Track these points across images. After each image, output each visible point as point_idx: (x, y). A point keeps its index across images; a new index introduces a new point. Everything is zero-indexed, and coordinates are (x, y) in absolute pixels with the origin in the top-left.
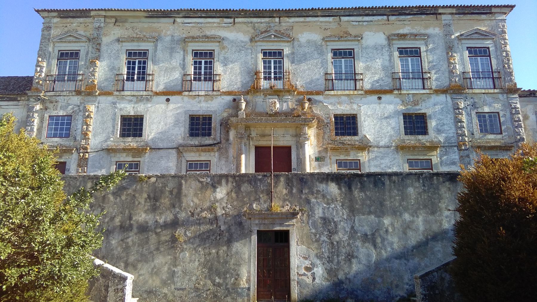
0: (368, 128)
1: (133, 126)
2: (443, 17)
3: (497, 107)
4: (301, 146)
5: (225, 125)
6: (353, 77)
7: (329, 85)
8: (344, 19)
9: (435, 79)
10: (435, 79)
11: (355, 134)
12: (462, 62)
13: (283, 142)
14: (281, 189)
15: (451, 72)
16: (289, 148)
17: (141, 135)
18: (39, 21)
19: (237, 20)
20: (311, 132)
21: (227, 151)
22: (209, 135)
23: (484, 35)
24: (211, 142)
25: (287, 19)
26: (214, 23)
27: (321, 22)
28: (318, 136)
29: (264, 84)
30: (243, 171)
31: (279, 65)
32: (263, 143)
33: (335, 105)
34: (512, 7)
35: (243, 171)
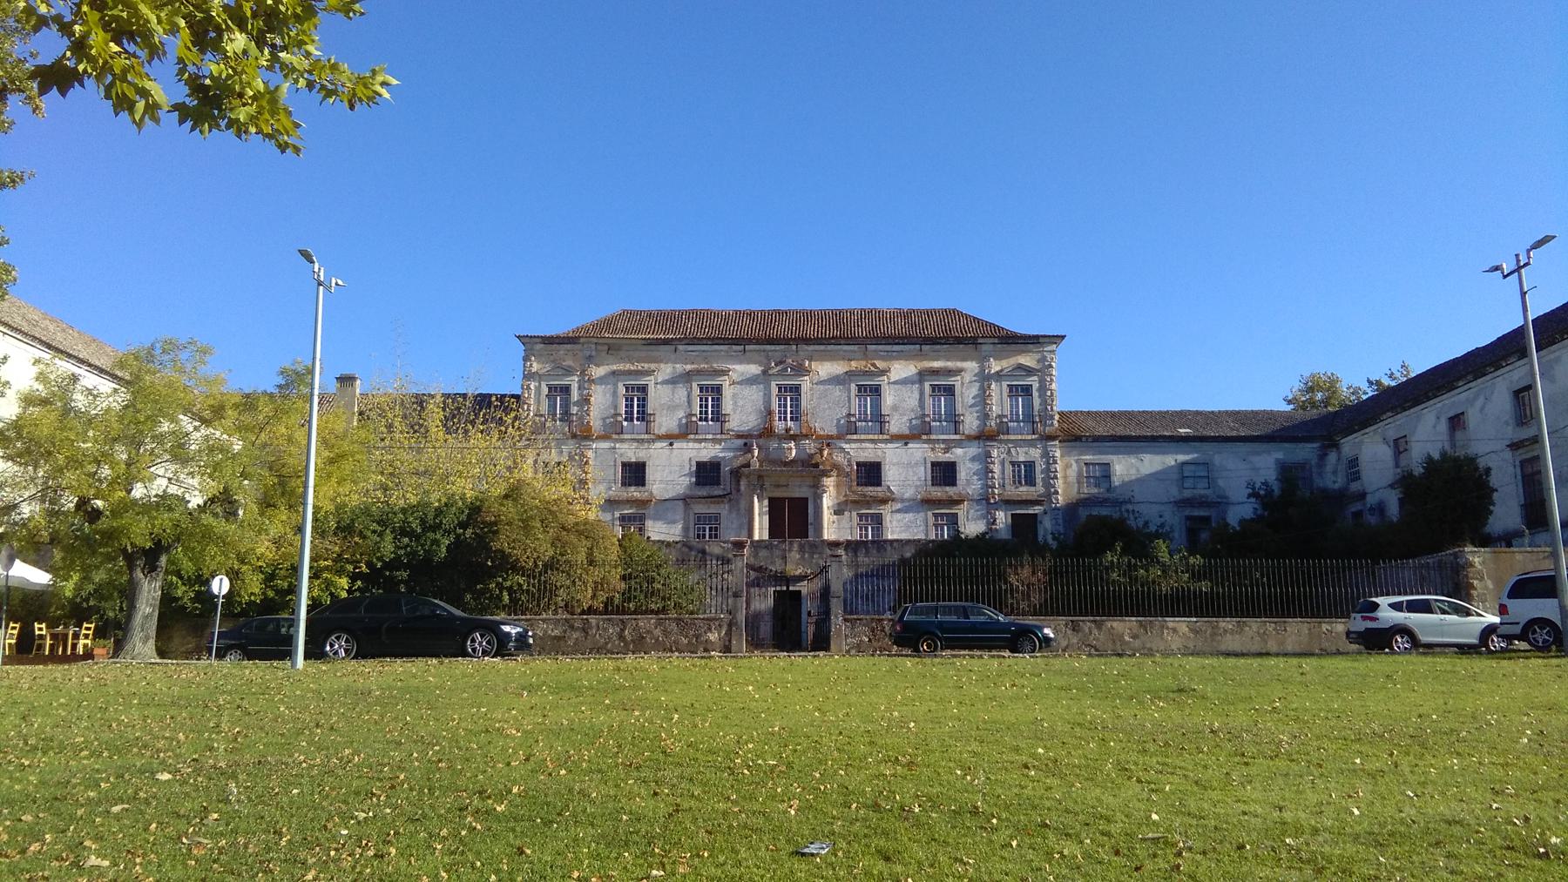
0: (893, 477)
1: (635, 473)
2: (984, 347)
3: (1035, 453)
4: (818, 498)
5: (736, 474)
6: (879, 419)
7: (849, 429)
9: (971, 423)
10: (971, 423)
11: (879, 484)
12: (999, 401)
13: (797, 493)
14: (795, 555)
15: (986, 416)
16: (806, 499)
17: (643, 485)
18: (520, 349)
20: (829, 482)
21: (738, 502)
22: (718, 484)
23: (1029, 371)
28: (838, 486)
29: (779, 426)
30: (756, 537)
31: (796, 402)
32: (778, 494)
33: (858, 451)
34: (1063, 337)
35: (756, 537)
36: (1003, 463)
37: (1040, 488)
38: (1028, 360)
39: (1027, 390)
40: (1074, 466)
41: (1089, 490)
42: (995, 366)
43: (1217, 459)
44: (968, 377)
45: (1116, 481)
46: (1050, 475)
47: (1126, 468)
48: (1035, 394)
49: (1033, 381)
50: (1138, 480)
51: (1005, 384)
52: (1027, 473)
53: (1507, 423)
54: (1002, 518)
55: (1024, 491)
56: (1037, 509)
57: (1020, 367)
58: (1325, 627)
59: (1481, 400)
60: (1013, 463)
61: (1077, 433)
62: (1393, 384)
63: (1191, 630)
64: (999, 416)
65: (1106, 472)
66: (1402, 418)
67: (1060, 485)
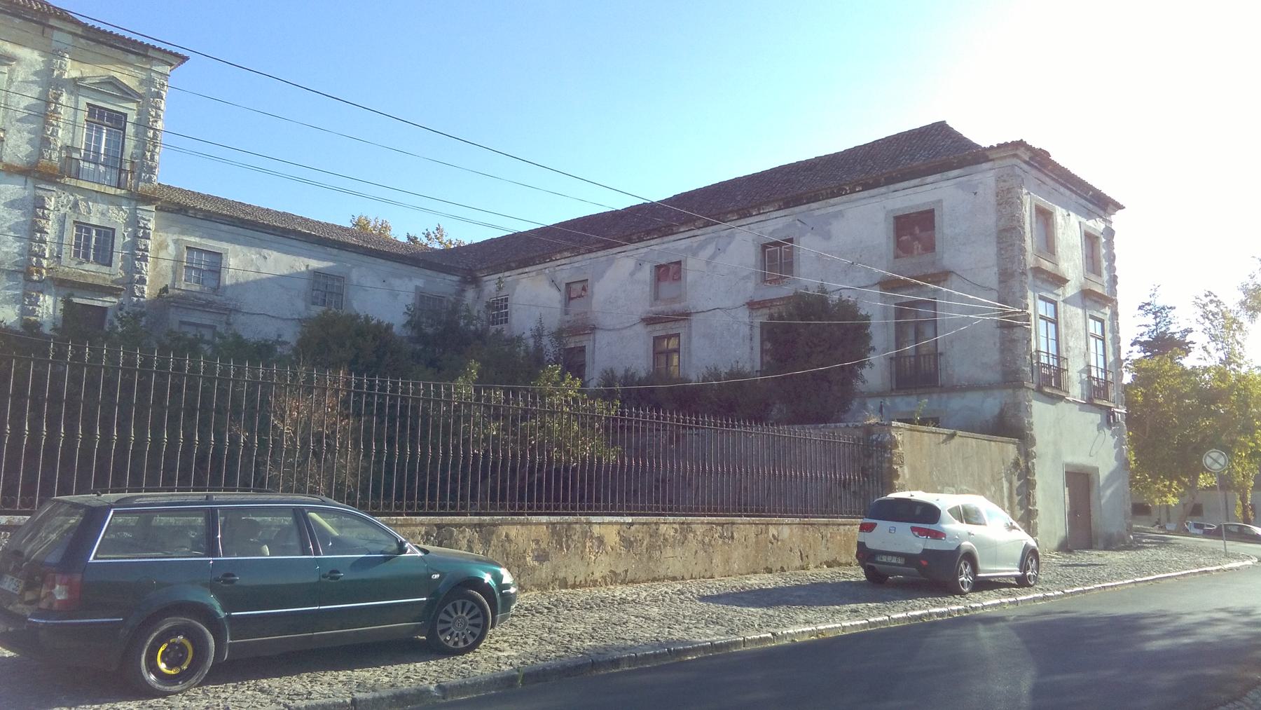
2: (57, 35)
3: (117, 217)
15: (45, 142)
23: (126, 93)
34: (184, 59)
36: (62, 222)
37: (117, 269)
38: (128, 77)
39: (118, 121)
40: (172, 249)
41: (186, 285)
42: (72, 70)
43: (355, 275)
44: (21, 73)
45: (228, 279)
46: (136, 253)
47: (243, 263)
48: (130, 129)
49: (131, 110)
50: (255, 282)
51: (83, 102)
52: (99, 244)
53: (746, 278)
54: (47, 306)
55: (91, 270)
56: (109, 301)
57: (113, 82)
58: (772, 530)
59: (710, 250)
60: (79, 225)
61: (183, 209)
62: (437, 246)
63: (623, 539)
64: (69, 148)
65: (216, 262)
66: (583, 261)
67: (148, 269)
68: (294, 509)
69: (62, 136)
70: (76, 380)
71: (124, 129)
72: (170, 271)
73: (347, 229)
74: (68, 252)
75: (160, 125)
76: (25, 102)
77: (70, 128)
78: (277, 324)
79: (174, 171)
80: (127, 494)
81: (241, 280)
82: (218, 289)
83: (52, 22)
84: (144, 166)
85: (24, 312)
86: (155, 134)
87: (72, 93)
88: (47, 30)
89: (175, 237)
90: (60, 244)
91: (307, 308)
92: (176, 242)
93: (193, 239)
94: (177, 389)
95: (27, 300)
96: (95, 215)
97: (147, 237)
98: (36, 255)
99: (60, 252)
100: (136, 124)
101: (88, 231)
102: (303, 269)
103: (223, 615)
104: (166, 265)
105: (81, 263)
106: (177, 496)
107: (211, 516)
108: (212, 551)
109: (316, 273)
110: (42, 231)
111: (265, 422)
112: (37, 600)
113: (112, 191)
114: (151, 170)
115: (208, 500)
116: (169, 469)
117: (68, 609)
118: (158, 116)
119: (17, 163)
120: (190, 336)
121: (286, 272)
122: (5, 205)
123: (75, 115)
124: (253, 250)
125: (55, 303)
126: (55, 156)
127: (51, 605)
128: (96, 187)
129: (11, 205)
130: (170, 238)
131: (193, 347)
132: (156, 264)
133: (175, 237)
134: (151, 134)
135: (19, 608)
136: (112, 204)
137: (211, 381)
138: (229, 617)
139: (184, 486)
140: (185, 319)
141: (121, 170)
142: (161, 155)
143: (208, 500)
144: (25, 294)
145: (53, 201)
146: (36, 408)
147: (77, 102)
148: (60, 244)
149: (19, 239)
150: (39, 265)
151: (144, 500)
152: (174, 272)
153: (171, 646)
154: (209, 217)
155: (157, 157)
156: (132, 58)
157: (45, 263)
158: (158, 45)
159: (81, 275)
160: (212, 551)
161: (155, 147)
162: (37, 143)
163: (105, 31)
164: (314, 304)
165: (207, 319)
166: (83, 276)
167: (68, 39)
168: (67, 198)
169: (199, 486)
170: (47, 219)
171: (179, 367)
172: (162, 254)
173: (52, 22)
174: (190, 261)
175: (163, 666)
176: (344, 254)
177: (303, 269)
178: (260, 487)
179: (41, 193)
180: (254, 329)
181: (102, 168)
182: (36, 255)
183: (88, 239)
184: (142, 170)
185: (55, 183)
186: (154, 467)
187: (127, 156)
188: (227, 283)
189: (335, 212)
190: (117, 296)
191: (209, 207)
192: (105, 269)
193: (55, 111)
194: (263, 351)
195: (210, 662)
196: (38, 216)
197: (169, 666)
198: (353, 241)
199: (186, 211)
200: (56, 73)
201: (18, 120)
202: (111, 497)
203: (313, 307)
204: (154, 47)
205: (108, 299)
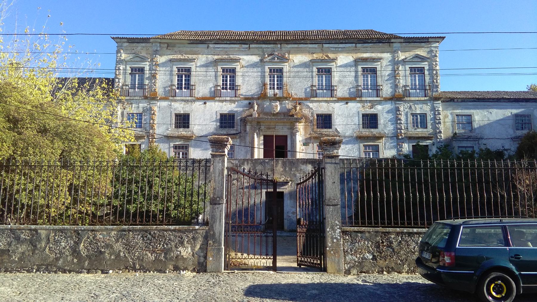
2: (395, 45)
3: (426, 109)
8: (324, 45)
15: (396, 86)
19: (251, 46)
23: (423, 59)
24: (235, 132)
25: (286, 46)
26: (236, 48)
27: (310, 48)
36: (406, 115)
38: (422, 52)
39: (421, 70)
40: (450, 117)
42: (402, 56)
45: (476, 125)
46: (436, 121)
47: (481, 117)
48: (426, 73)
49: (425, 65)
51: (407, 67)
52: (421, 120)
54: (406, 148)
55: (420, 131)
56: (428, 142)
57: (417, 56)
60: (413, 115)
61: (451, 100)
64: (405, 86)
65: (469, 119)
67: (442, 127)
68: (502, 226)
69: (402, 82)
70: (426, 174)
71: (424, 73)
72: (451, 126)
73: (527, 92)
74: (410, 126)
75: (438, 68)
76: (388, 73)
77: (405, 79)
78: (503, 141)
79: (445, 85)
80: (467, 220)
81: (482, 125)
82: (472, 130)
83: (393, 40)
84: (434, 86)
85: (398, 151)
86: (436, 72)
87: (403, 65)
88: (391, 44)
89: (451, 112)
90: (407, 124)
91: (514, 132)
92: (451, 114)
93: (458, 111)
94: (466, 175)
95: (398, 146)
96: (418, 109)
97: (439, 114)
98: (399, 129)
99: (407, 126)
100: (429, 70)
101: (417, 116)
102: (510, 114)
103: (517, 273)
104: (449, 124)
105: (416, 129)
106: (488, 220)
107: (504, 228)
108: (508, 244)
109: (516, 115)
110: (400, 120)
111: (515, 187)
112: (438, 262)
113: (423, 99)
114: (437, 87)
115: (501, 222)
116: (469, 209)
117: (451, 266)
118: (436, 64)
119: (388, 96)
120: (470, 152)
121: (502, 118)
122: (386, 112)
123: (405, 73)
124: (485, 110)
125: (409, 146)
126: (400, 90)
127: (444, 264)
128: (417, 99)
129: (388, 112)
130: (448, 113)
131: (471, 156)
132: (445, 125)
133: (451, 112)
134: (435, 72)
135: (430, 264)
136: (424, 104)
137: (381, 169)
138: (520, 274)
139: (490, 215)
140: (460, 145)
141: (425, 90)
142: (441, 80)
143: (501, 222)
144: (398, 144)
145: (403, 107)
146: (413, 186)
147: (405, 68)
148: (407, 124)
149: (392, 124)
150: (401, 132)
151: (474, 222)
152: (453, 126)
153: (496, 285)
154: (463, 100)
155: (438, 81)
156: (423, 44)
157: (403, 131)
158: (432, 35)
159: (416, 134)
160: (508, 244)
161: (437, 77)
162: (394, 87)
163: (411, 38)
164: (517, 129)
165: (468, 144)
166: (417, 134)
167: (399, 45)
168: (407, 105)
169: (497, 216)
170: (401, 115)
171: (466, 165)
172: (447, 120)
173: (393, 40)
174: (458, 120)
175: (494, 294)
176: (529, 104)
177: (510, 114)
178: (517, 215)
179: (397, 105)
180: (495, 145)
181: (418, 91)
182: (399, 129)
183: (417, 119)
184: (433, 88)
185: (402, 101)
186: (462, 209)
187: (427, 84)
188: (476, 127)
189: (519, 85)
190: (431, 140)
191: (462, 96)
192: (425, 130)
193: (398, 74)
194: (499, 155)
195: (515, 294)
196: (398, 114)
197: (497, 294)
198: (532, 97)
199: (454, 100)
200: (396, 59)
201: (386, 80)
202: (460, 221)
203: (518, 131)
204: (431, 37)
205: (428, 141)
